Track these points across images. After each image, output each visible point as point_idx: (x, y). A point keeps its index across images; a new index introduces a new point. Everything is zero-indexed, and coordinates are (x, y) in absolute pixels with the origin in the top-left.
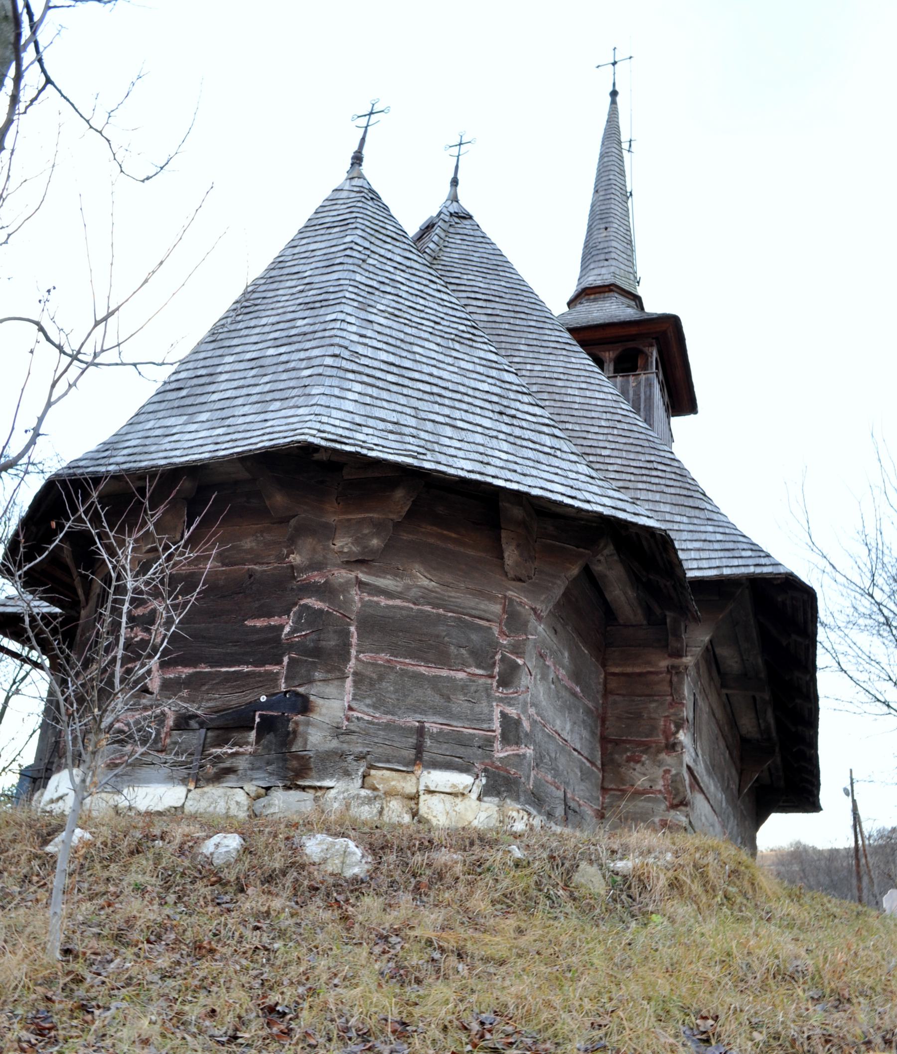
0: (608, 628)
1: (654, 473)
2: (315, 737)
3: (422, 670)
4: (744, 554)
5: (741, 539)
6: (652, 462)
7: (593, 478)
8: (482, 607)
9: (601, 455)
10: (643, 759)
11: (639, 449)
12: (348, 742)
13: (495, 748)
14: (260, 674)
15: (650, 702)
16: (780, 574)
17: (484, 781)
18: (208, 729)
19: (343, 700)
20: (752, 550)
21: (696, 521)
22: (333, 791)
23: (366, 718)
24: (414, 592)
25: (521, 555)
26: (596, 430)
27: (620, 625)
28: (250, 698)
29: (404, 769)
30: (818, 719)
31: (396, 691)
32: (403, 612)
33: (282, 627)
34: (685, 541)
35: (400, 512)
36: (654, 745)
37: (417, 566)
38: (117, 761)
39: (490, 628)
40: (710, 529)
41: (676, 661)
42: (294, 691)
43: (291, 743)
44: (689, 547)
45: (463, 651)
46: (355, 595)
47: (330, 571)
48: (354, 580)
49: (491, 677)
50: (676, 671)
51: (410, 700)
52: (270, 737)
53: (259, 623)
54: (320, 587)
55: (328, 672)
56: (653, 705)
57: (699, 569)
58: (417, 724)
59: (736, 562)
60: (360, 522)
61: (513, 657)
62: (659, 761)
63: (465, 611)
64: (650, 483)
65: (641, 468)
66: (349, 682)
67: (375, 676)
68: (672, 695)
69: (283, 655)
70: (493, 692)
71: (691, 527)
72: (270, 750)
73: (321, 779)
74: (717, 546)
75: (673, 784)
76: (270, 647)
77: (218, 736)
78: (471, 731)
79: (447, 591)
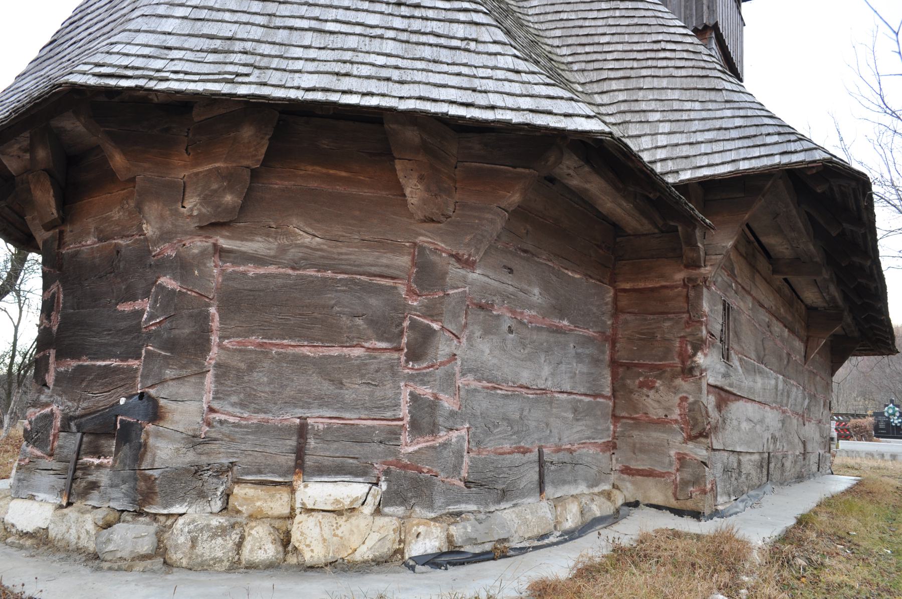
0: (618, 240)
1: (662, 55)
2: (165, 451)
3: (306, 351)
4: (769, 140)
5: (771, 121)
6: (659, 42)
7: (518, 72)
8: (384, 261)
9: (598, 44)
10: (657, 385)
11: (644, 29)
12: (207, 454)
13: (403, 441)
15: (665, 320)
16: (814, 162)
17: (384, 486)
19: (201, 400)
20: (779, 134)
21: (710, 106)
22: (181, 521)
23: (231, 419)
24: (293, 253)
25: (428, 190)
26: (595, 14)
27: (630, 235)
28: (112, 400)
29: (281, 480)
30: (886, 293)
31: (270, 383)
34: (695, 132)
35: (255, 156)
36: (669, 369)
37: (295, 220)
39: (395, 288)
40: (729, 113)
41: (694, 273)
44: (699, 140)
45: (359, 321)
46: (215, 269)
47: (181, 241)
48: (211, 249)
49: (398, 349)
50: (694, 285)
51: (289, 392)
54: (172, 261)
55: (183, 367)
56: (667, 324)
57: (709, 166)
58: (298, 421)
59: (756, 152)
61: (426, 322)
62: (675, 387)
63: (361, 269)
64: (656, 67)
65: (646, 51)
66: (209, 378)
67: (243, 366)
68: (688, 312)
70: (400, 369)
71: (704, 114)
72: (125, 465)
74: (734, 134)
75: (691, 414)
78: (369, 423)
79: (336, 247)
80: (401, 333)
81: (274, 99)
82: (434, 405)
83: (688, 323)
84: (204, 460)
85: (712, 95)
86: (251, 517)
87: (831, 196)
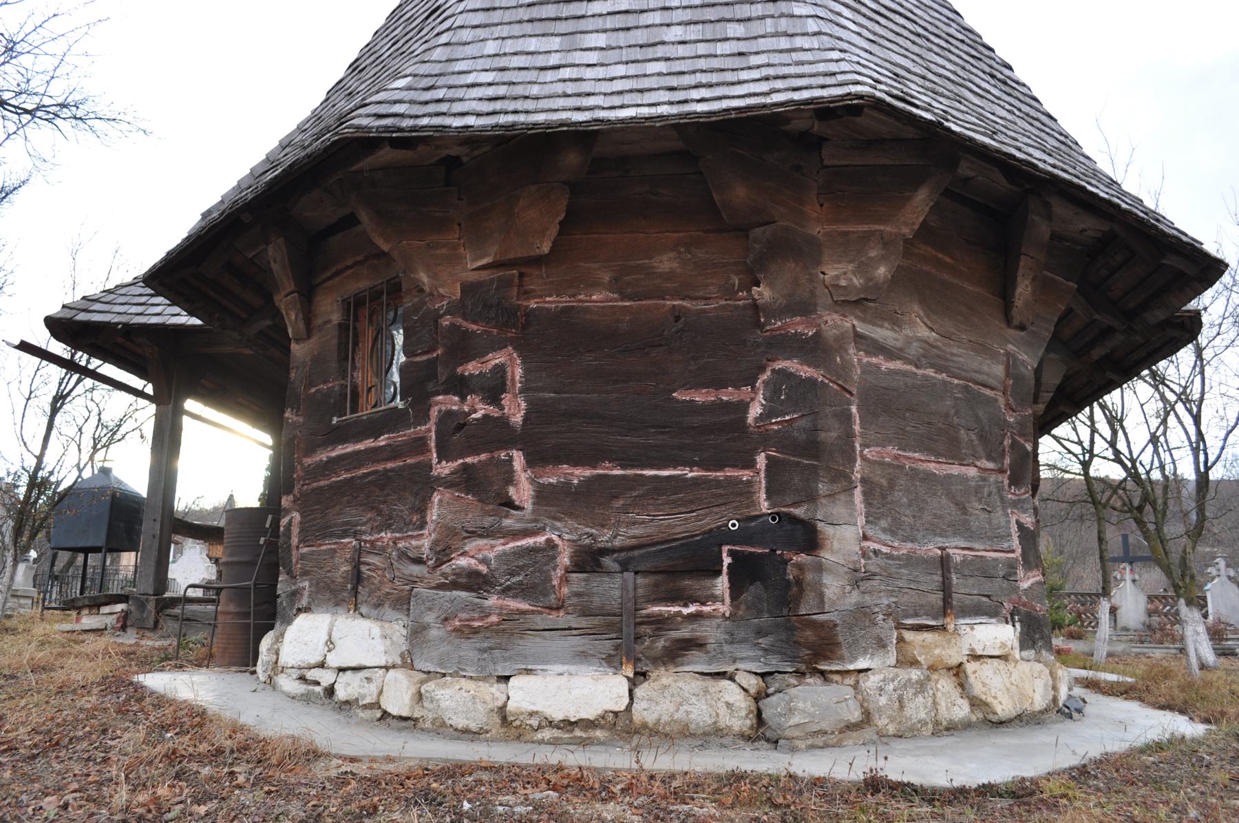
2: (835, 593)
3: (932, 467)
12: (870, 592)
14: (717, 483)
18: (636, 573)
19: (855, 525)
23: (885, 550)
32: (908, 380)
33: (743, 407)
37: (916, 307)
38: (476, 624)
39: (996, 400)
42: (787, 514)
43: (798, 599)
46: (855, 356)
52: (754, 591)
53: (700, 397)
58: (939, 552)
60: (865, 238)
66: (858, 492)
67: (884, 482)
69: (753, 452)
73: (854, 659)
76: (725, 438)
77: (656, 585)
86: (932, 668)
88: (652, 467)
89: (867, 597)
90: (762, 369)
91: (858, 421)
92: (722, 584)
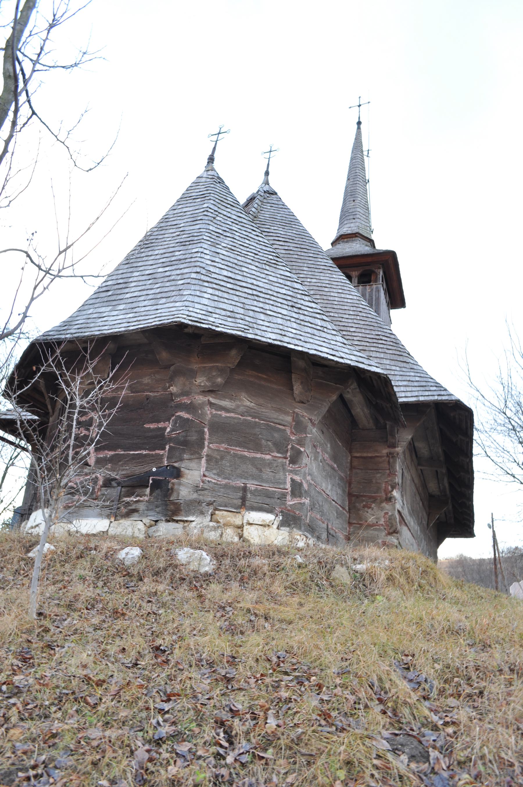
1: (380, 342)
2: (184, 492)
3: (246, 454)
4: (432, 388)
7: (345, 344)
8: (281, 418)
11: (372, 328)
14: (152, 455)
15: (377, 473)
17: (281, 518)
18: (122, 487)
19: (200, 470)
21: (404, 369)
22: (194, 523)
23: (213, 481)
24: (242, 409)
26: (347, 316)
28: (147, 469)
31: (230, 466)
33: (165, 429)
37: (243, 394)
40: (412, 374)
41: (392, 450)
43: (170, 495)
45: (269, 443)
46: (208, 411)
48: (207, 402)
49: (286, 458)
50: (392, 456)
51: (239, 471)
52: (158, 492)
53: (152, 426)
54: (187, 405)
55: (192, 454)
56: (379, 475)
57: (406, 397)
59: (427, 393)
61: (298, 447)
66: (204, 461)
67: (218, 457)
68: (389, 469)
69: (166, 444)
71: (401, 373)
72: (158, 499)
74: (416, 384)
76: (158, 440)
77: (128, 491)
80: (287, 451)
81: (263, 342)
82: (301, 485)
83: (389, 475)
84: (201, 497)
85: (405, 365)
87: (447, 429)
88: (133, 451)
89: (201, 497)
90: (173, 415)
91: (208, 434)
92: (148, 490)
